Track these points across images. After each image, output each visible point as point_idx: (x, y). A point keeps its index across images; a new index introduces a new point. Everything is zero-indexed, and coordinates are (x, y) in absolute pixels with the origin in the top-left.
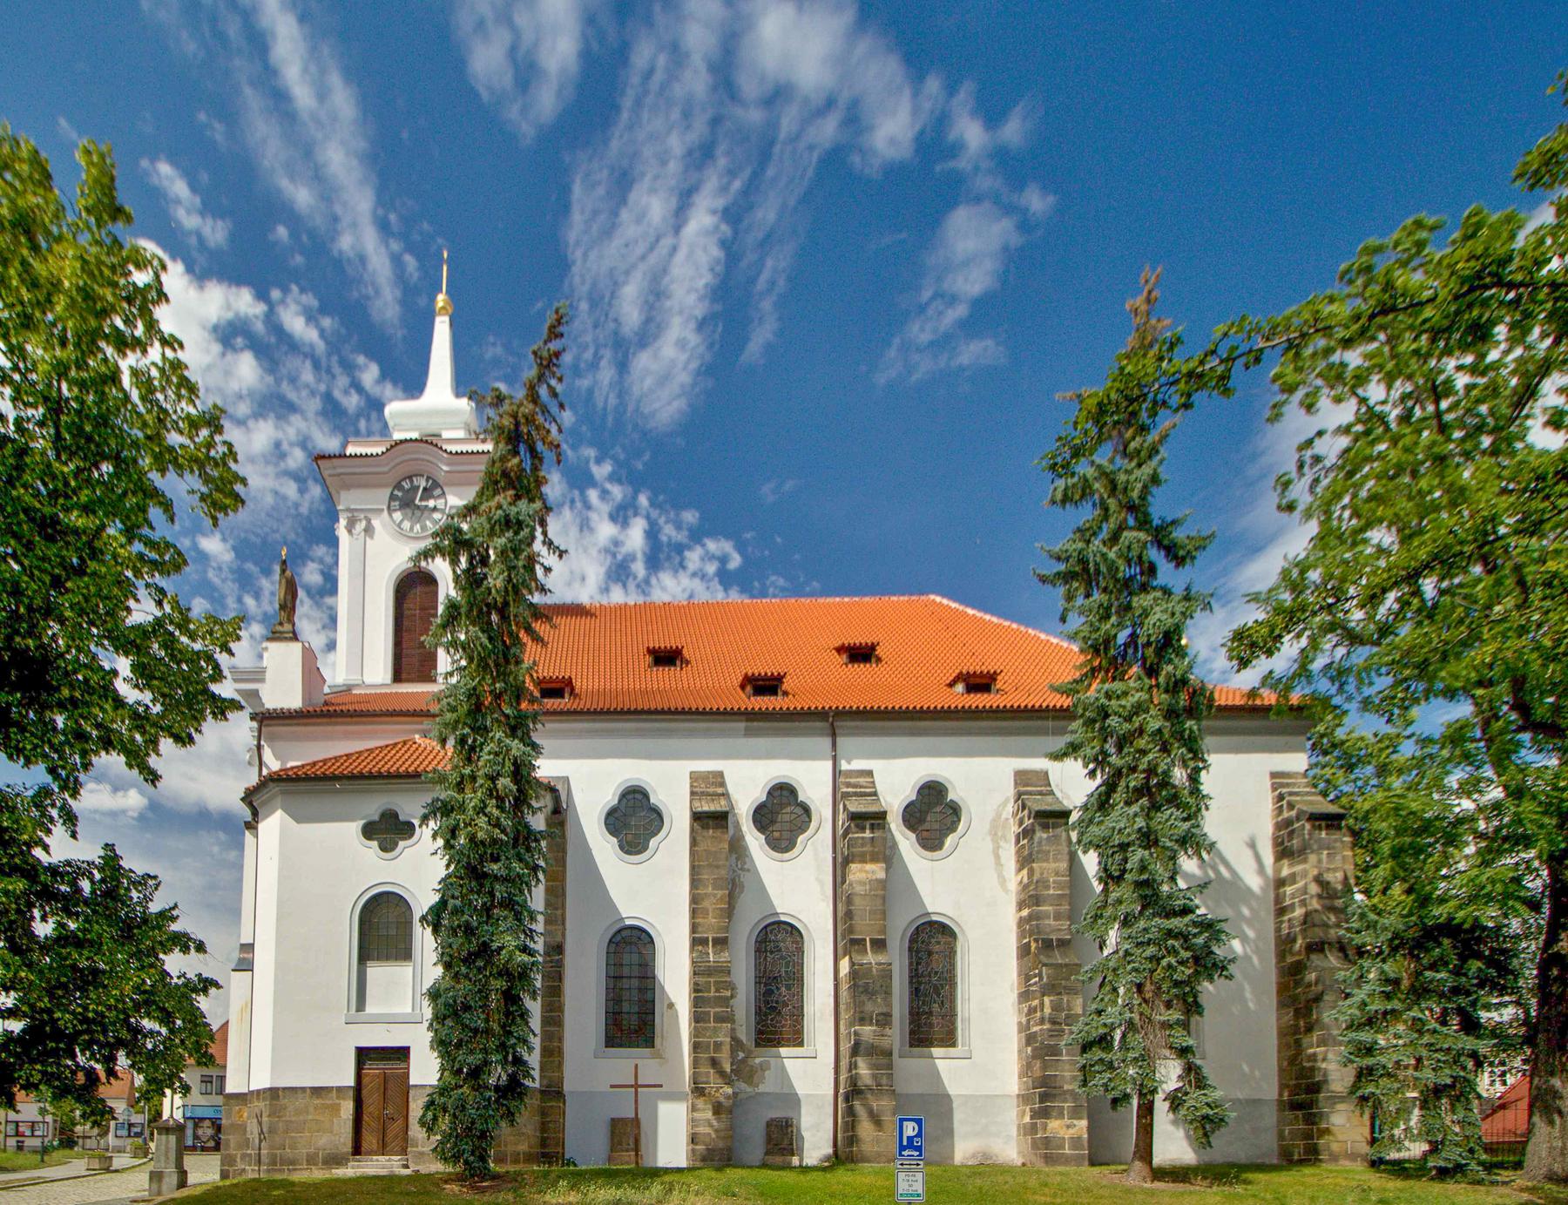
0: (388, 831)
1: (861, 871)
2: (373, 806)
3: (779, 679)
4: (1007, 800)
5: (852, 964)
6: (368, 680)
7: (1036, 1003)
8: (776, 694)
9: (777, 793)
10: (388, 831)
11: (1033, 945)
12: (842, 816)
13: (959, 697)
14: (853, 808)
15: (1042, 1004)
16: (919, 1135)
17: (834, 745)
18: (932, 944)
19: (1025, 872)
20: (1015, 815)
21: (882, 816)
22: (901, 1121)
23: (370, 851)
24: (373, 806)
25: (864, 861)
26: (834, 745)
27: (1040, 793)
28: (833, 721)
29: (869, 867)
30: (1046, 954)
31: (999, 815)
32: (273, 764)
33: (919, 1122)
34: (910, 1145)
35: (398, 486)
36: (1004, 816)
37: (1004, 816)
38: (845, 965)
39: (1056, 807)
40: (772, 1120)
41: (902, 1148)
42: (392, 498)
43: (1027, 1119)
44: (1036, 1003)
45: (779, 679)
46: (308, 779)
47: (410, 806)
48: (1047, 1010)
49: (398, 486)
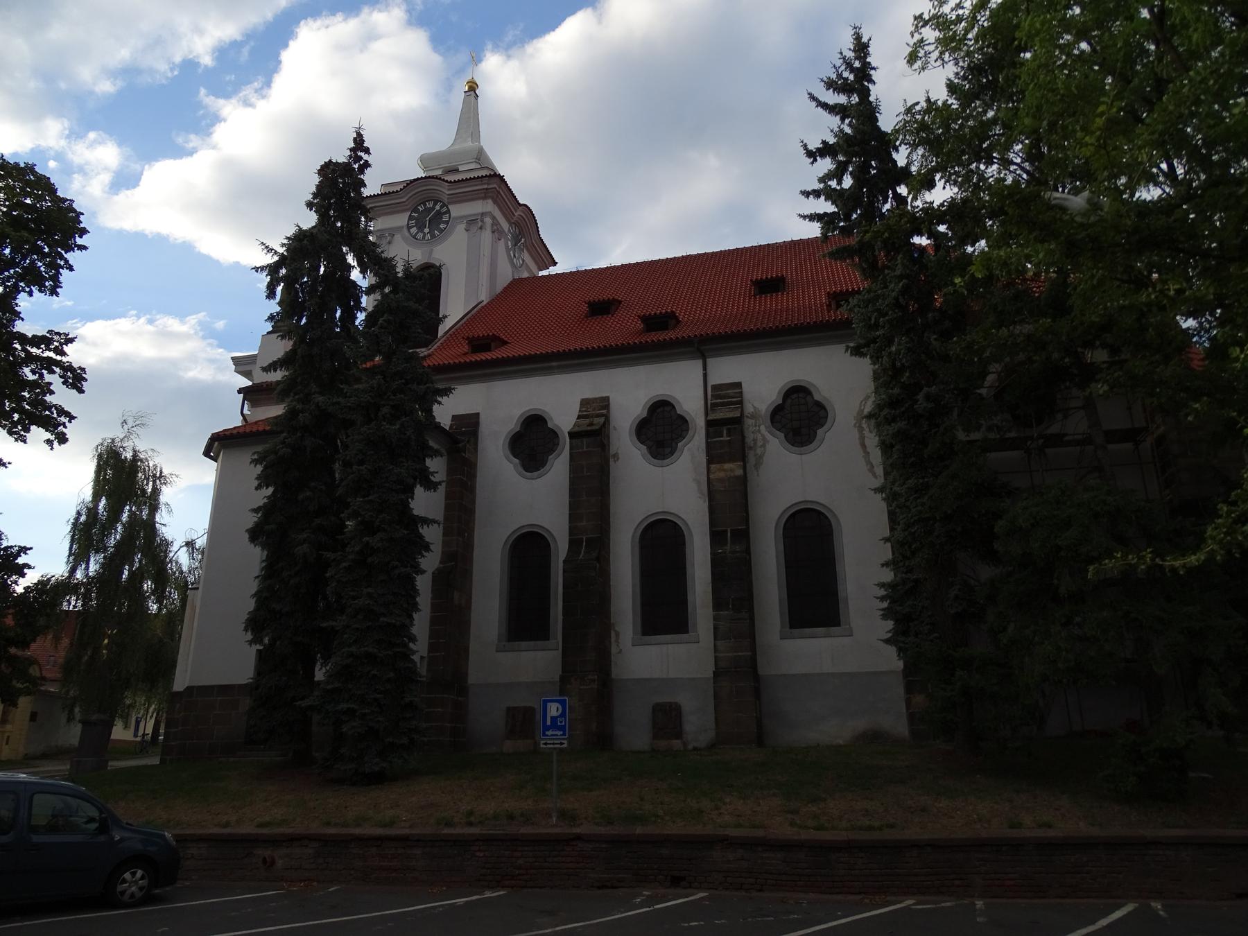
4: (868, 397)
22: (546, 702)
26: (705, 368)
29: (727, 466)
35: (415, 210)
42: (410, 218)
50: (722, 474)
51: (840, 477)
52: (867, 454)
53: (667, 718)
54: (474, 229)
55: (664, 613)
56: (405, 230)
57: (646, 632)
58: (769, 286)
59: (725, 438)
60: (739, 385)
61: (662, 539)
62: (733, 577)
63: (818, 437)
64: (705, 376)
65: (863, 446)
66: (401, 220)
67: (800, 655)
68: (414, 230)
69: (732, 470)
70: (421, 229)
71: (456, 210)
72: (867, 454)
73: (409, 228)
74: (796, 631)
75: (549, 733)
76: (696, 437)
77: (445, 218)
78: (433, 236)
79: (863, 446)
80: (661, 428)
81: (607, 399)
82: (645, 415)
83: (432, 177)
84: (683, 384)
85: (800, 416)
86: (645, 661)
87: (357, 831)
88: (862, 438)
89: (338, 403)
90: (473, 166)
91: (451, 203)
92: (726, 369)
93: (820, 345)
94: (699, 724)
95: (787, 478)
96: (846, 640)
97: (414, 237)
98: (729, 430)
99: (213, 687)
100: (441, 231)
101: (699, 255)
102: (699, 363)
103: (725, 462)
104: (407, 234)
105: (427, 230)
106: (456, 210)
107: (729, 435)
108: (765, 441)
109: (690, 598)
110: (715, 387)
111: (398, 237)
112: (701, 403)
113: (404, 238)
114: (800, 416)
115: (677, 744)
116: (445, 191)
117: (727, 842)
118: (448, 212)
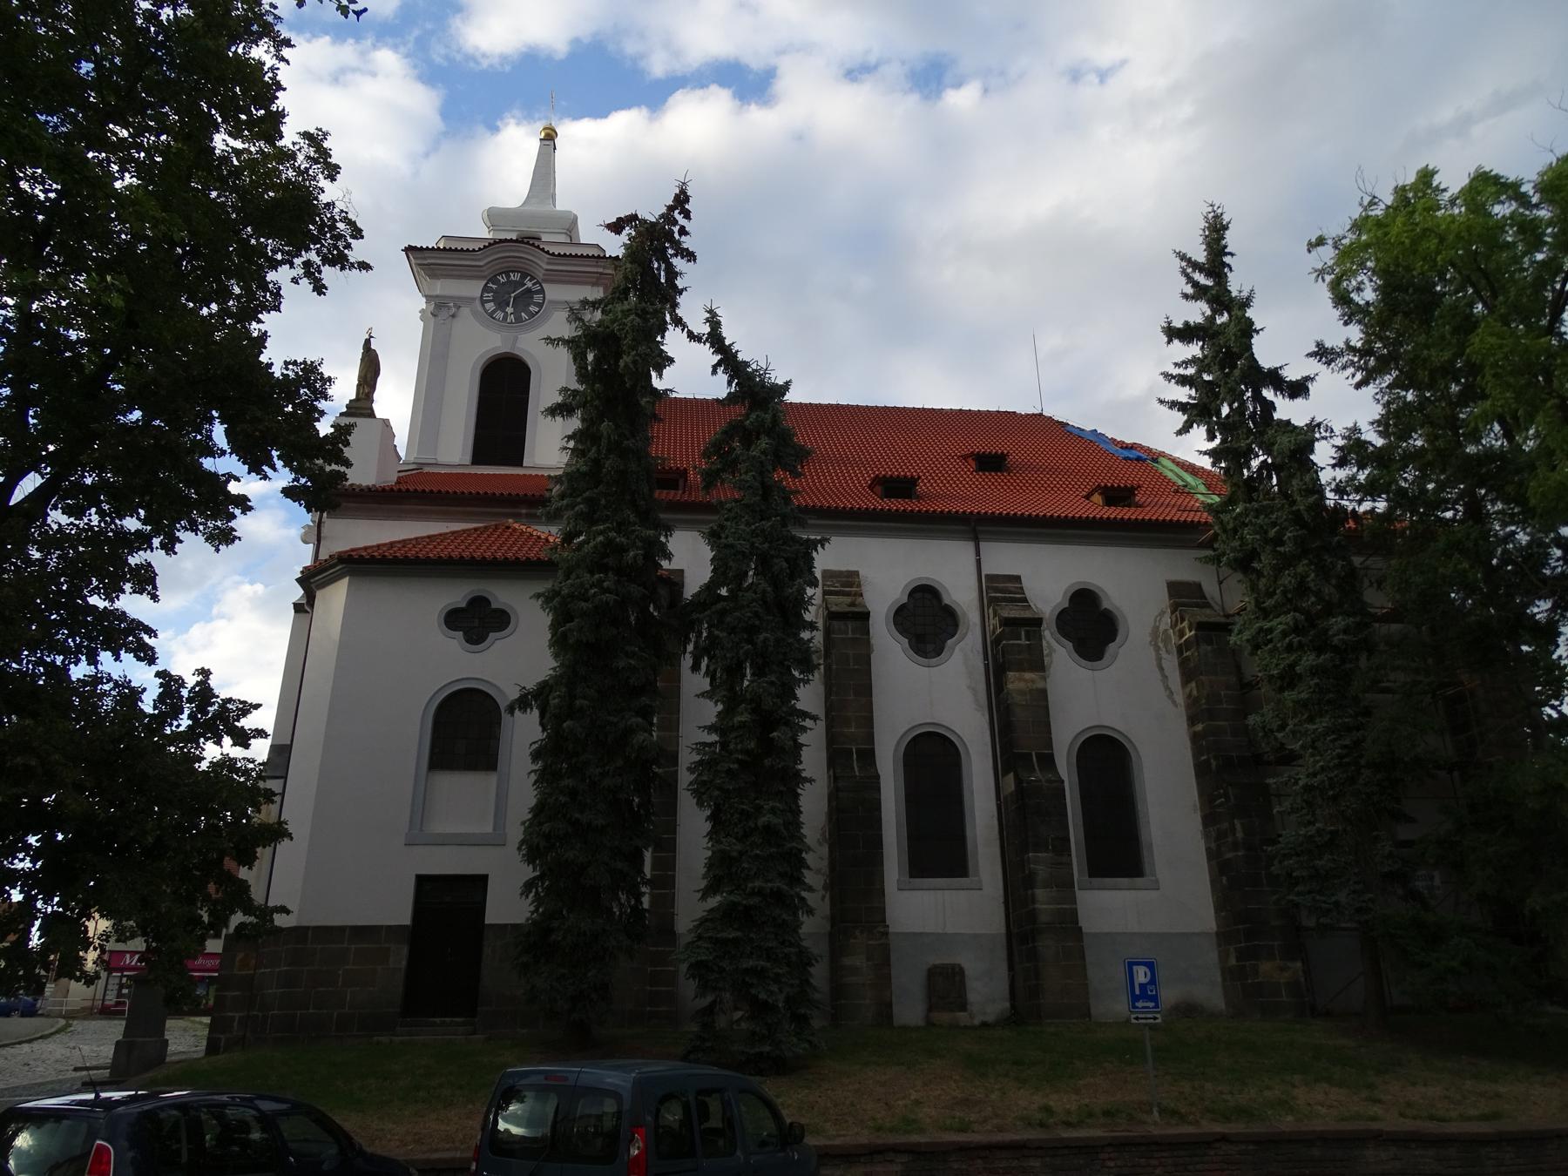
0: (478, 622)
1: (1020, 679)
2: (456, 594)
3: (913, 482)
4: (1162, 613)
5: (1018, 781)
6: (442, 459)
7: (1225, 825)
8: (910, 497)
9: (918, 595)
10: (478, 622)
11: (1214, 763)
12: (993, 622)
13: (1096, 508)
14: (1005, 614)
15: (1233, 830)
16: (1153, 981)
17: (978, 553)
18: (1106, 757)
19: (1193, 684)
20: (1173, 626)
21: (865, 616)
22: (1131, 965)
23: (454, 643)
24: (456, 594)
25: (1021, 669)
26: (978, 553)
27: (1197, 605)
28: (976, 527)
29: (1028, 675)
30: (1232, 773)
31: (1156, 629)
32: (333, 547)
33: (1150, 966)
34: (1144, 995)
35: (493, 280)
36: (1162, 629)
37: (1162, 629)
38: (1010, 783)
39: (1027, 615)
40: (935, 967)
41: (1135, 998)
42: (486, 289)
43: (1233, 961)
44: (1225, 825)
45: (913, 482)
46: (395, 561)
47: (504, 594)
48: (1240, 835)
49: (493, 280)
50: (1022, 685)
51: (1129, 697)
52: (1165, 677)
53: (946, 985)
54: (444, 314)
55: (938, 853)
56: (478, 303)
57: (963, 872)
58: (991, 463)
59: (1023, 642)
60: (1017, 579)
61: (932, 755)
62: (1027, 815)
63: (1107, 656)
64: (979, 562)
65: (1161, 669)
66: (474, 288)
67: (1106, 908)
68: (490, 306)
69: (1033, 681)
70: (501, 305)
71: (553, 292)
72: (1165, 677)
73: (483, 302)
74: (1097, 881)
75: (1140, 1004)
76: (969, 635)
77: (537, 298)
78: (519, 319)
79: (1161, 669)
80: (926, 619)
81: (856, 573)
82: (905, 600)
83: (501, 241)
84: (953, 568)
85: (1090, 625)
86: (918, 910)
87: (1067, 1134)
88: (1159, 659)
89: (732, 546)
90: (563, 238)
91: (546, 281)
92: (1005, 557)
93: (1141, 546)
94: (987, 991)
95: (1081, 697)
96: (1154, 894)
97: (491, 315)
98: (1027, 633)
99: (342, 929)
100: (532, 315)
101: (838, 406)
102: (970, 546)
103: (1024, 671)
104: (480, 308)
105: (510, 310)
106: (553, 292)
107: (1028, 639)
108: (1052, 650)
109: (969, 833)
110: (990, 578)
111: (465, 311)
112: (974, 595)
113: (475, 313)
114: (1090, 625)
115: (962, 1017)
116: (542, 265)
117: (1381, 1139)
118: (542, 291)
